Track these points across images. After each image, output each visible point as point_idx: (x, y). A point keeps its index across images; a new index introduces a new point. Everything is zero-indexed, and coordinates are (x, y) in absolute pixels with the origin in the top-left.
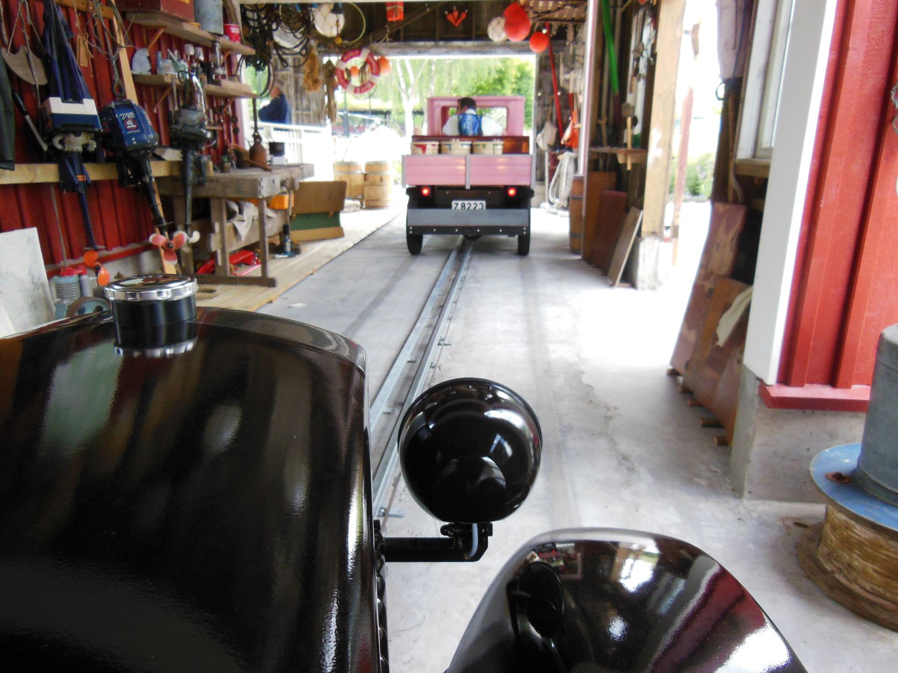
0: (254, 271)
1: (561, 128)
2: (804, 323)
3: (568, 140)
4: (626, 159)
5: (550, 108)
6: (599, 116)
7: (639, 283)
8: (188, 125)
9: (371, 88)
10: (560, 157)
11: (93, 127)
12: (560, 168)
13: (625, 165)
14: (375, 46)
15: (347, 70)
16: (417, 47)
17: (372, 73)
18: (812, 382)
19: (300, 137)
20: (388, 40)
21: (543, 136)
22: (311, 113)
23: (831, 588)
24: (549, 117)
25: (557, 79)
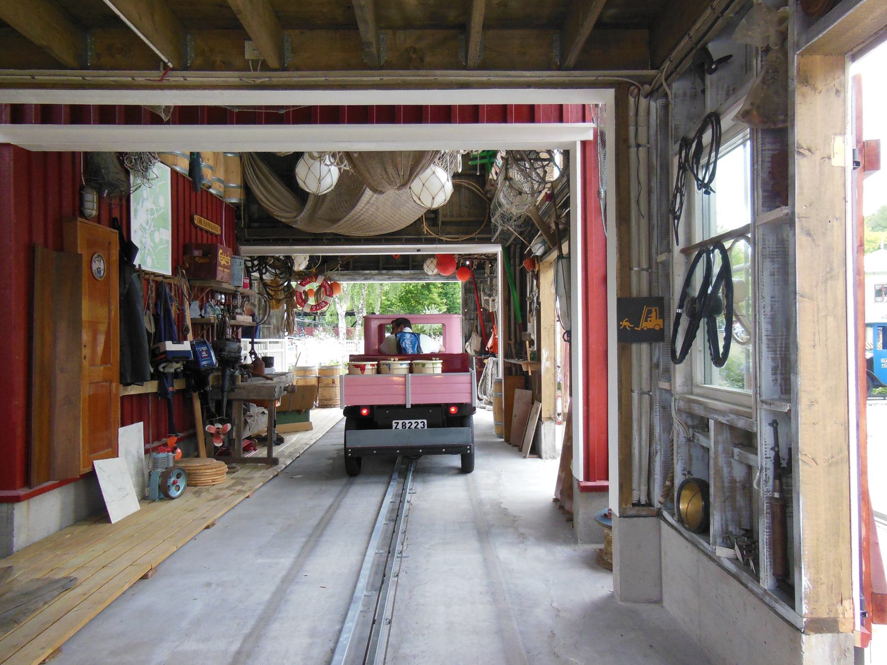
0: (262, 452)
1: (485, 338)
2: (591, 451)
3: (491, 348)
4: (528, 368)
5: (476, 321)
6: (510, 339)
7: (544, 455)
8: (232, 352)
9: (325, 306)
10: (485, 361)
11: (188, 357)
12: (486, 370)
13: (527, 372)
14: (329, 273)
15: (304, 291)
16: (363, 275)
17: (326, 295)
18: (600, 480)
19: (266, 349)
20: (340, 269)
21: (470, 344)
22: (272, 326)
23: (604, 564)
24: (475, 328)
25: (479, 298)
